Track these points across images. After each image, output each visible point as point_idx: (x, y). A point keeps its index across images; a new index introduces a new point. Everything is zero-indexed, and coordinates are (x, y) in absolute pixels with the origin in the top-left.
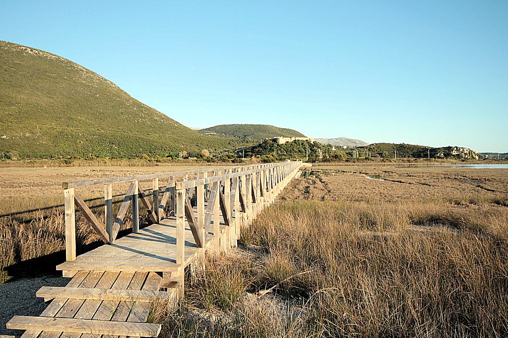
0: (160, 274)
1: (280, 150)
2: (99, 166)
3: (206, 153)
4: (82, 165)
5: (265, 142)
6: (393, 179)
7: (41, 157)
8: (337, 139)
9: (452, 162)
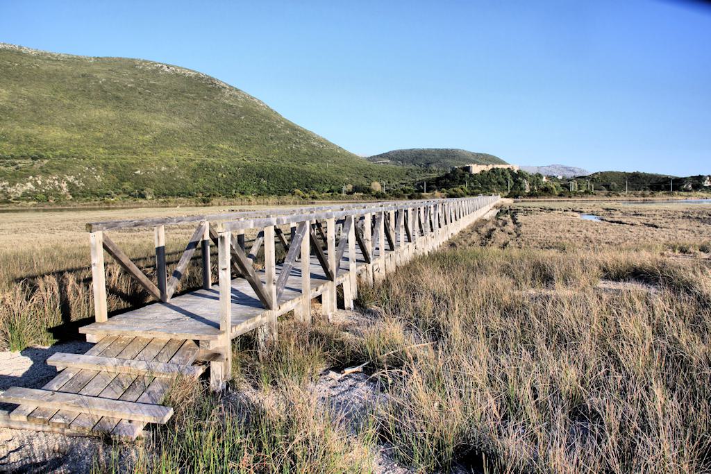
0: (197, 342)
1: (473, 181)
2: (242, 204)
3: (377, 186)
4: (222, 204)
5: (454, 171)
6: (612, 219)
7: (178, 195)
8: (549, 167)
9: (702, 196)
